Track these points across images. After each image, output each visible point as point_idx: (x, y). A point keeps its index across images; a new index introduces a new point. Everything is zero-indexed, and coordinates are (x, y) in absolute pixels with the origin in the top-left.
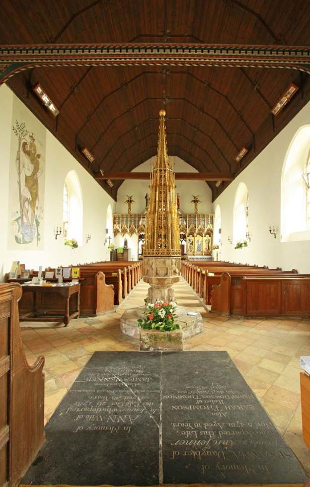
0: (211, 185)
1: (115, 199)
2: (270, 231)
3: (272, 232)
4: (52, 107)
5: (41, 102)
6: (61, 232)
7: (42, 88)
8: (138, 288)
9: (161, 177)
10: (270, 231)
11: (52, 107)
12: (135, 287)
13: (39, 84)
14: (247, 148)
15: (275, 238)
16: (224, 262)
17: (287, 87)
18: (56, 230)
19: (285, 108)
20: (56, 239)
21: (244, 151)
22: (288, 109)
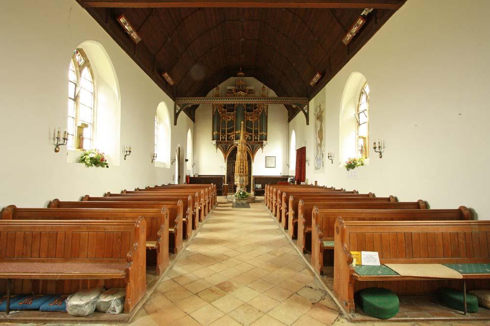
0: (288, 107)
1: (194, 121)
2: (375, 148)
3: (377, 149)
4: (134, 35)
5: (124, 30)
6: (130, 152)
7: (126, 18)
8: (200, 235)
9: (243, 163)
10: (375, 148)
11: (134, 35)
12: (193, 232)
13: (123, 14)
14: (320, 74)
15: (381, 157)
16: (332, 189)
17: (315, 74)
18: (52, 137)
19: (354, 38)
20: (125, 159)
21: (318, 75)
22: (362, 34)
